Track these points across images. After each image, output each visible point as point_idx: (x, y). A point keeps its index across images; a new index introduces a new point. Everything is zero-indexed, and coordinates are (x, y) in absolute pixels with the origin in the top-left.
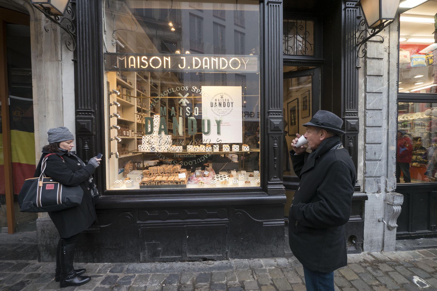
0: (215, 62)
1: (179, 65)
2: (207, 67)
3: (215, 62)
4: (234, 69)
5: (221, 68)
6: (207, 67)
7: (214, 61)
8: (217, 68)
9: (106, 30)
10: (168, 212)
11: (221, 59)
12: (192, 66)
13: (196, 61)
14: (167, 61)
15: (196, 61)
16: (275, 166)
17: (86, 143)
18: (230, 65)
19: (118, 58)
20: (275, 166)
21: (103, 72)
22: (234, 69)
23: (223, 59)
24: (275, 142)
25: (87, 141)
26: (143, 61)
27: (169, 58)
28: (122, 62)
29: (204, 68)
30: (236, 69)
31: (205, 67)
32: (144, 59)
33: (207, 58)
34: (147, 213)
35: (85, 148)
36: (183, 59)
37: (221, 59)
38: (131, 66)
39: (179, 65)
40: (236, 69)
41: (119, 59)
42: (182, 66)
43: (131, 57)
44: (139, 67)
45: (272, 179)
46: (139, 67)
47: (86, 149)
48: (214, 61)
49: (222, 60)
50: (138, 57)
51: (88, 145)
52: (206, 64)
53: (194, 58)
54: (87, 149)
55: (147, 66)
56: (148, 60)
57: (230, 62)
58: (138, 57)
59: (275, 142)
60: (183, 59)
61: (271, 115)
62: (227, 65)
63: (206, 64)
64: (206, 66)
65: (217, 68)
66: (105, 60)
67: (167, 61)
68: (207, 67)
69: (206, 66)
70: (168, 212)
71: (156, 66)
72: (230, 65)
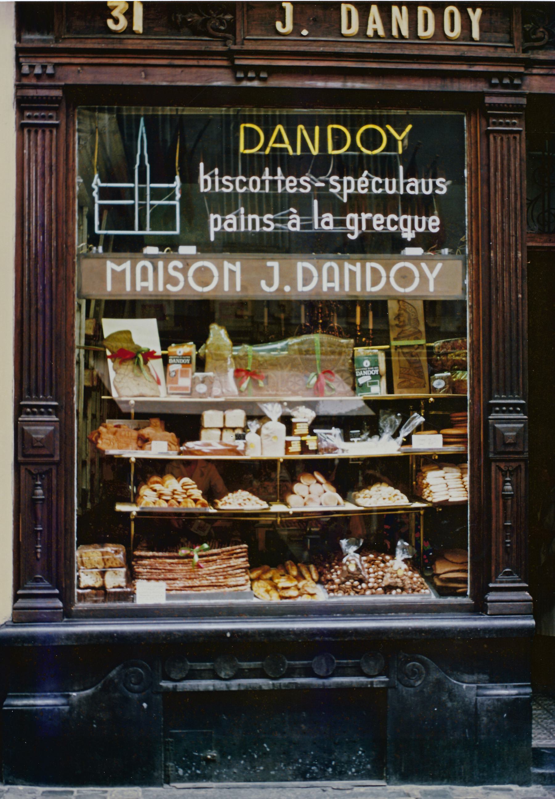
0: (352, 274)
3: (352, 274)
14: (232, 273)
32: (175, 268)
36: (272, 268)
41: (113, 271)
42: (270, 285)
52: (331, 279)
60: (272, 268)
63: (331, 279)
64: (331, 285)
67: (232, 273)
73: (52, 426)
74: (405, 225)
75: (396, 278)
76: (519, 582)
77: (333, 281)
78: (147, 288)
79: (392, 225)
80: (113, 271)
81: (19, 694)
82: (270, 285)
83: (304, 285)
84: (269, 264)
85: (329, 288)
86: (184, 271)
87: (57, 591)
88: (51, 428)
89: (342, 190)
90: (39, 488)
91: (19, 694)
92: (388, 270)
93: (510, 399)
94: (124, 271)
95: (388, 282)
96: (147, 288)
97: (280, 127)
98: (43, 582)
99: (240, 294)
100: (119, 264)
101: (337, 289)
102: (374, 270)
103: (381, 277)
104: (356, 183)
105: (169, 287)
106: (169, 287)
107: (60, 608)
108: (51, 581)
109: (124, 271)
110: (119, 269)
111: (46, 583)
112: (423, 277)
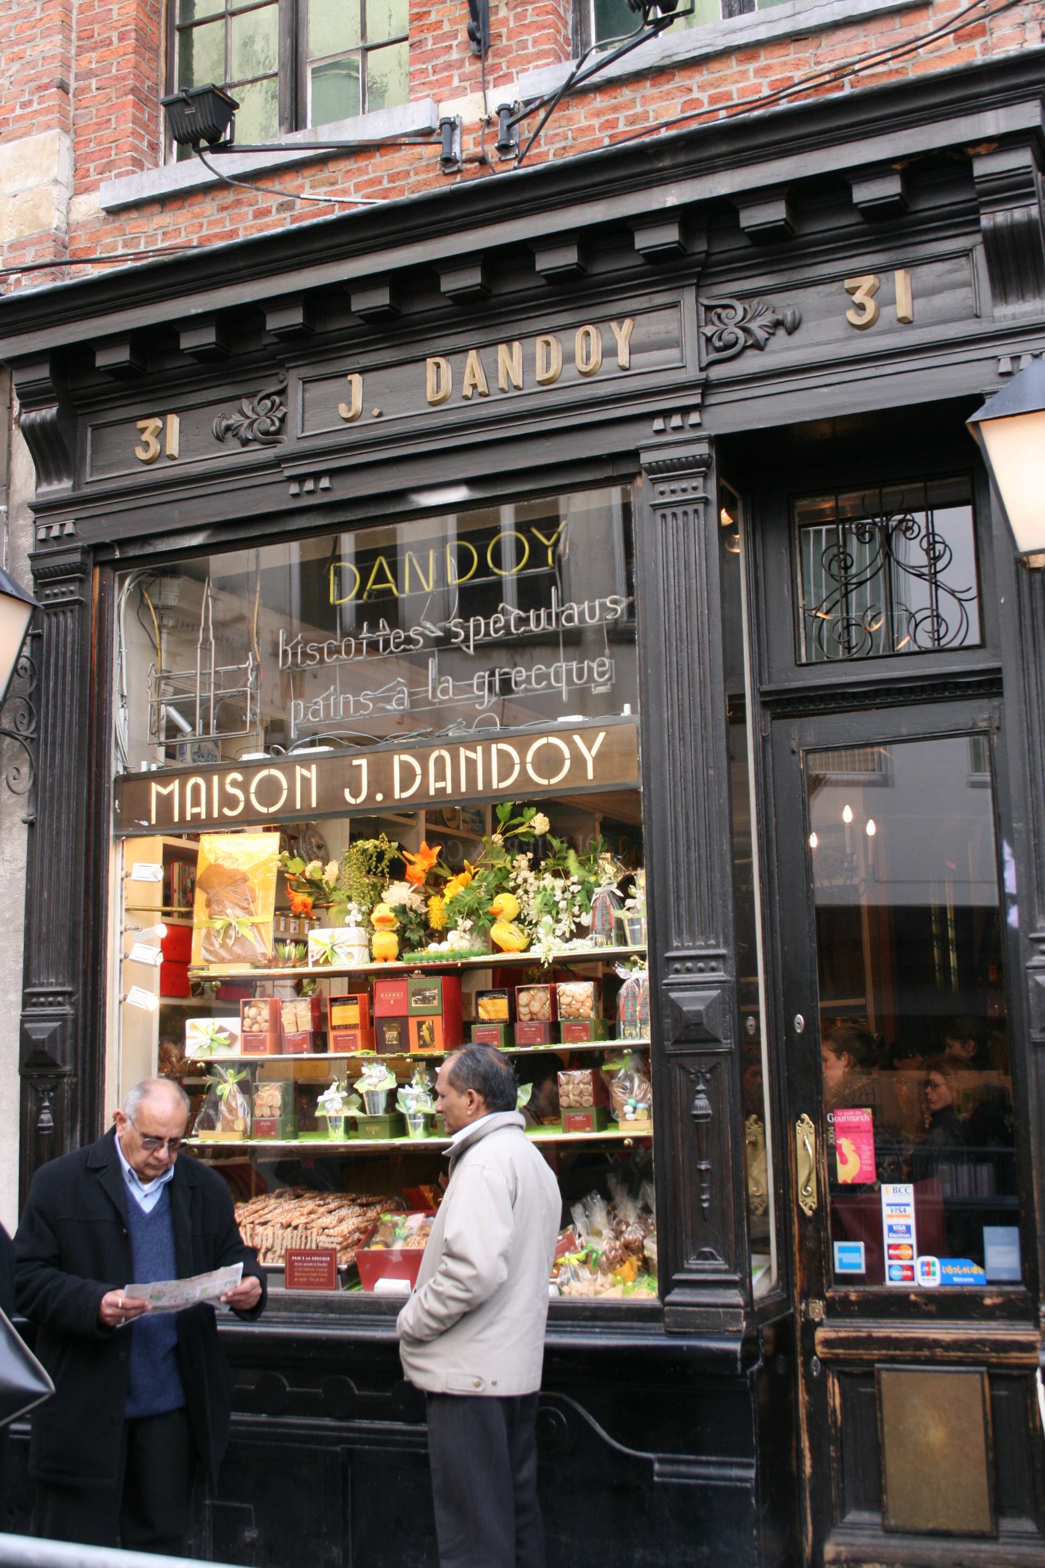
0: (471, 763)
1: (347, 791)
2: (199, 814)
3: (471, 763)
4: (545, 782)
5: (495, 786)
6: (445, 789)
7: (467, 758)
8: (480, 787)
9: (125, 694)
10: (286, 1383)
11: (494, 747)
12: (388, 794)
13: (406, 768)
14: (305, 781)
15: (406, 768)
16: (704, 1201)
17: (701, 1087)
18: (529, 768)
19: (155, 788)
20: (704, 1201)
21: (108, 844)
22: (545, 782)
23: (406, 758)
24: (699, 1092)
25: (50, 1100)
26: (230, 789)
27: (314, 767)
28: (165, 802)
29: (432, 792)
30: (553, 781)
31: (436, 790)
32: (234, 783)
33: (200, 781)
34: (353, 1384)
35: (42, 1121)
36: (360, 766)
37: (494, 747)
38: (436, 790)
39: (347, 791)
40: (553, 781)
41: (158, 794)
42: (355, 794)
43: (435, 755)
44: (216, 815)
45: (693, 1263)
46: (216, 815)
47: (45, 1125)
48: (467, 758)
49: (499, 751)
50: (216, 778)
51: (709, 1099)
52: (440, 776)
53: (396, 758)
54: (49, 1128)
55: (241, 806)
56: (244, 786)
57: (529, 758)
58: (216, 779)
59: (699, 1092)
60: (360, 766)
61: (677, 971)
62: (517, 768)
63: (440, 776)
64: (196, 810)
65: (480, 787)
66: (117, 802)
67: (305, 781)
68: (445, 789)
69: (196, 810)
70: (286, 1383)
71: (269, 805)
72: (529, 768)
73: (716, 988)
74: (558, 679)
75: (280, 789)
76: (726, 1272)
77: (444, 779)
78: (199, 814)
79: (538, 682)
80: (158, 794)
81: (266, 1429)
82: (355, 794)
83: (402, 790)
84: (355, 762)
85: (193, 815)
86: (244, 786)
87: (736, 1277)
88: (714, 993)
89: (467, 639)
90: (703, 1096)
91: (266, 1429)
92: (523, 754)
93: (688, 948)
94: (171, 795)
95: (248, 802)
96: (199, 814)
97: (382, 559)
98: (716, 1259)
99: (594, 784)
100: (165, 786)
101: (449, 791)
102: (503, 755)
103: (513, 765)
104: (487, 625)
105: (226, 811)
106: (226, 811)
107: (738, 1306)
108: (727, 1261)
109: (171, 795)
110: (165, 791)
111: (720, 1263)
112: (578, 760)
